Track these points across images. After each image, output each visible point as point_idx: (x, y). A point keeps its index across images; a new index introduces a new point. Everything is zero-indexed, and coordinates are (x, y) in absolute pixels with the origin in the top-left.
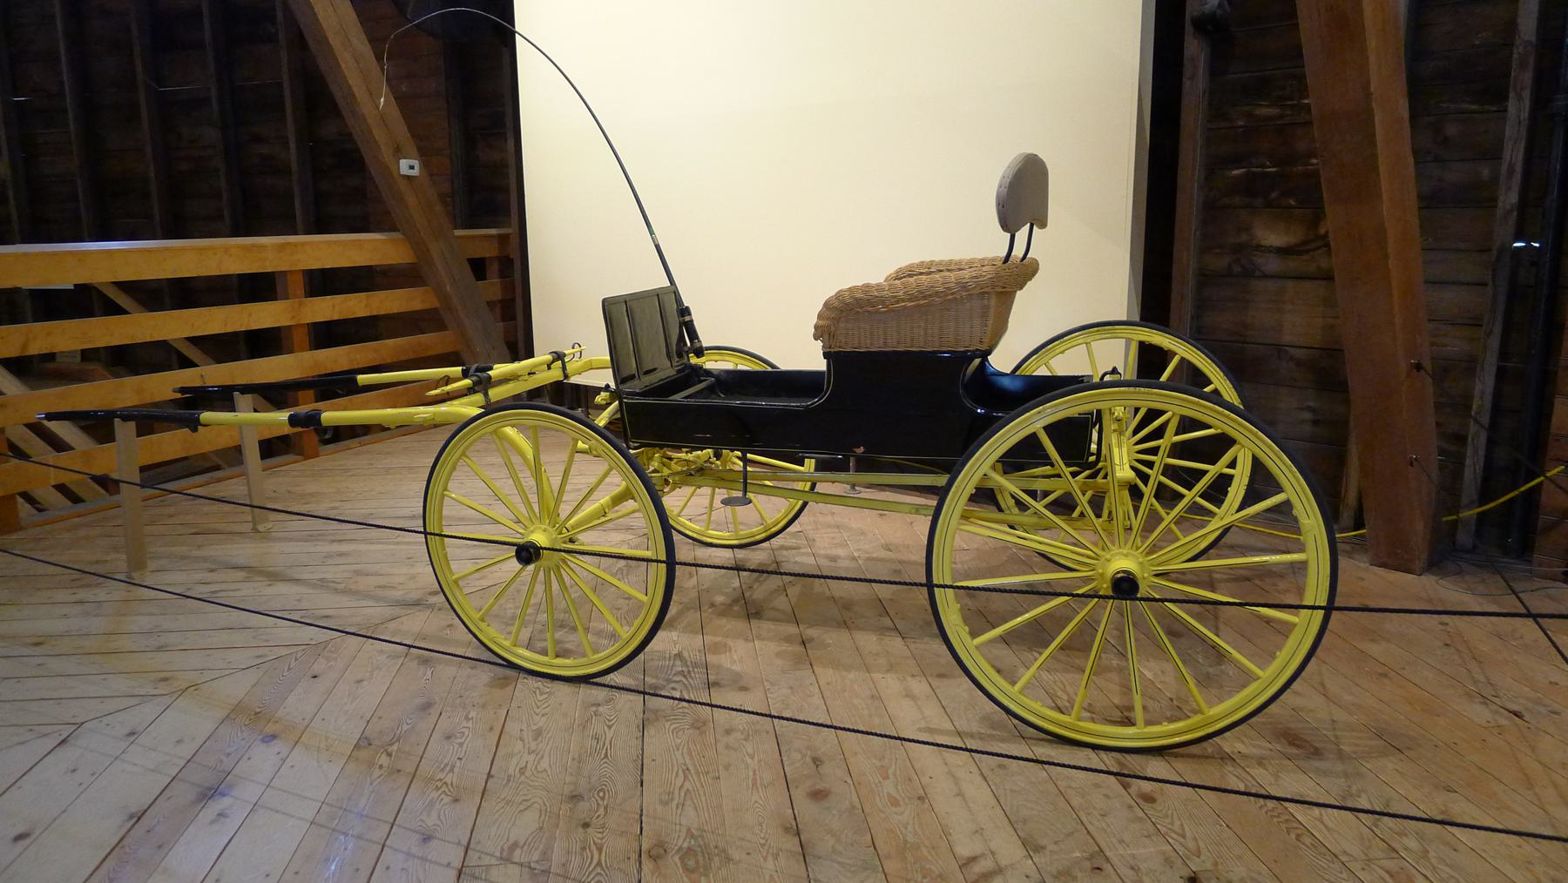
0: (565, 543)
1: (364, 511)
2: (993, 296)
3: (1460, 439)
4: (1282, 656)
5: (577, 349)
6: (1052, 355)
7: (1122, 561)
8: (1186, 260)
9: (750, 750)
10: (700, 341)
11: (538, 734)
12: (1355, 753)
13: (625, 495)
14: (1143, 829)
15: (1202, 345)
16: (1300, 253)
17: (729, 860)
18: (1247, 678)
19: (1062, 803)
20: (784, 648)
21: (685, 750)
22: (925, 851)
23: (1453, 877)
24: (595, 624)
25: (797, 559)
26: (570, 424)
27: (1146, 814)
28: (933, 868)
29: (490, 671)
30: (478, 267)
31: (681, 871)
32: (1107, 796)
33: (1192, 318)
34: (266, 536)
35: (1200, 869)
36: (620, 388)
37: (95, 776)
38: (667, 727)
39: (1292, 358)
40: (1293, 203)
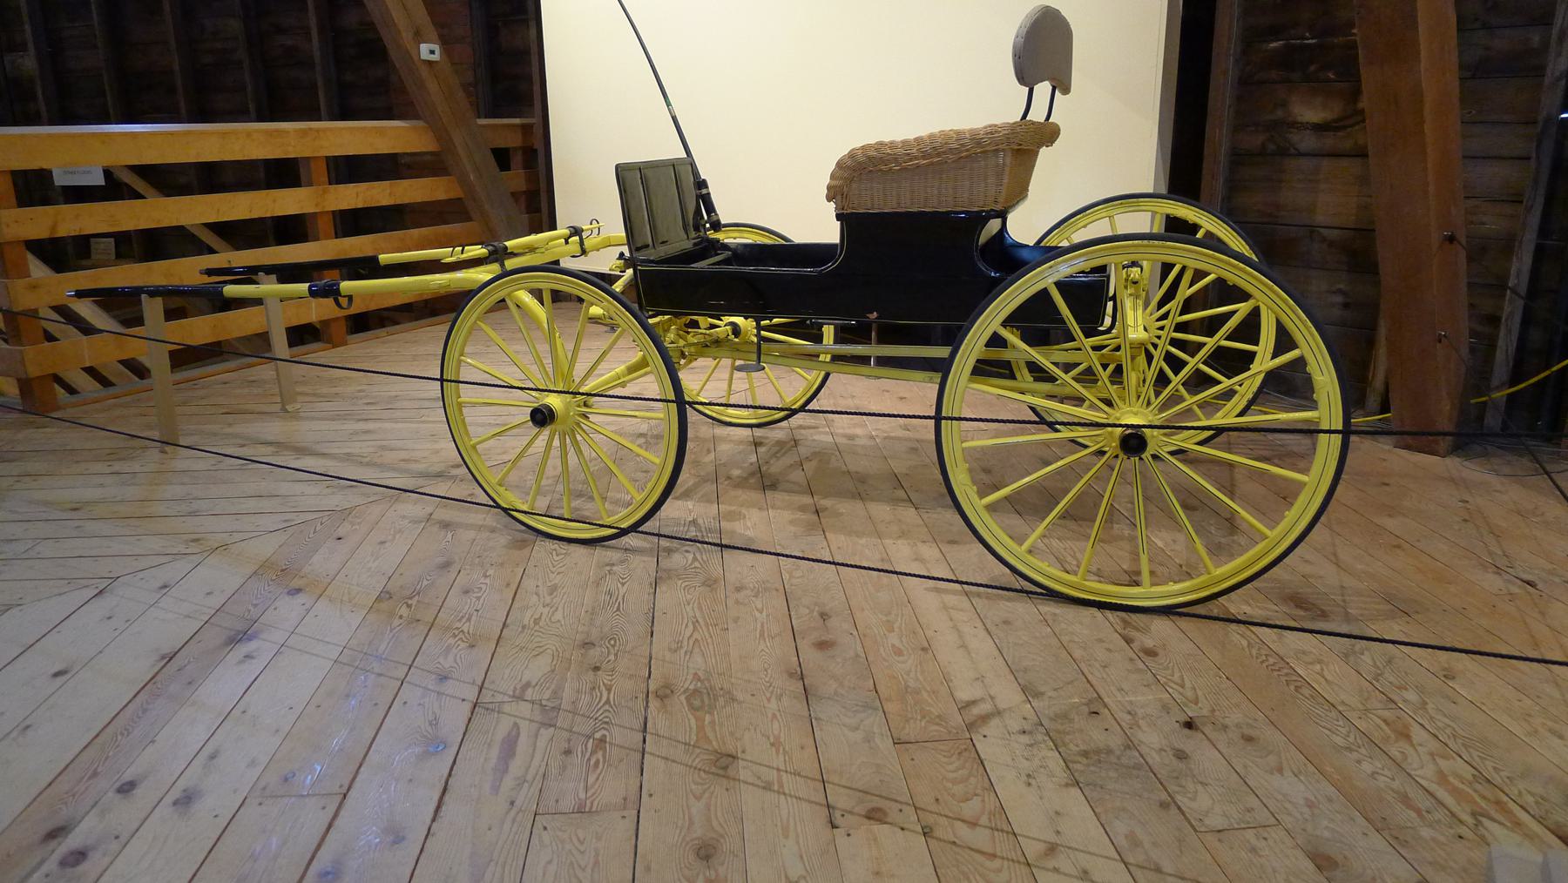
0: (579, 406)
1: (389, 393)
2: (1009, 154)
3: (1494, 320)
4: (1290, 515)
5: (595, 224)
6: (1074, 229)
7: (1132, 416)
8: (1219, 137)
9: (759, 606)
10: (716, 214)
11: (553, 590)
12: (1362, 615)
13: (642, 364)
14: (1143, 680)
15: (1240, 228)
16: (1337, 129)
17: (733, 700)
18: (1255, 538)
19: (1064, 654)
20: (797, 516)
21: (695, 605)
22: (925, 695)
23: (1449, 726)
24: (612, 494)
25: (814, 437)
26: (584, 287)
27: (1147, 666)
28: (932, 709)
29: (509, 535)
30: (502, 158)
31: (686, 709)
32: (1109, 650)
33: (1223, 199)
34: (295, 416)
35: (1196, 715)
36: (634, 255)
37: (130, 623)
38: (679, 585)
39: (1324, 239)
40: (1332, 77)
